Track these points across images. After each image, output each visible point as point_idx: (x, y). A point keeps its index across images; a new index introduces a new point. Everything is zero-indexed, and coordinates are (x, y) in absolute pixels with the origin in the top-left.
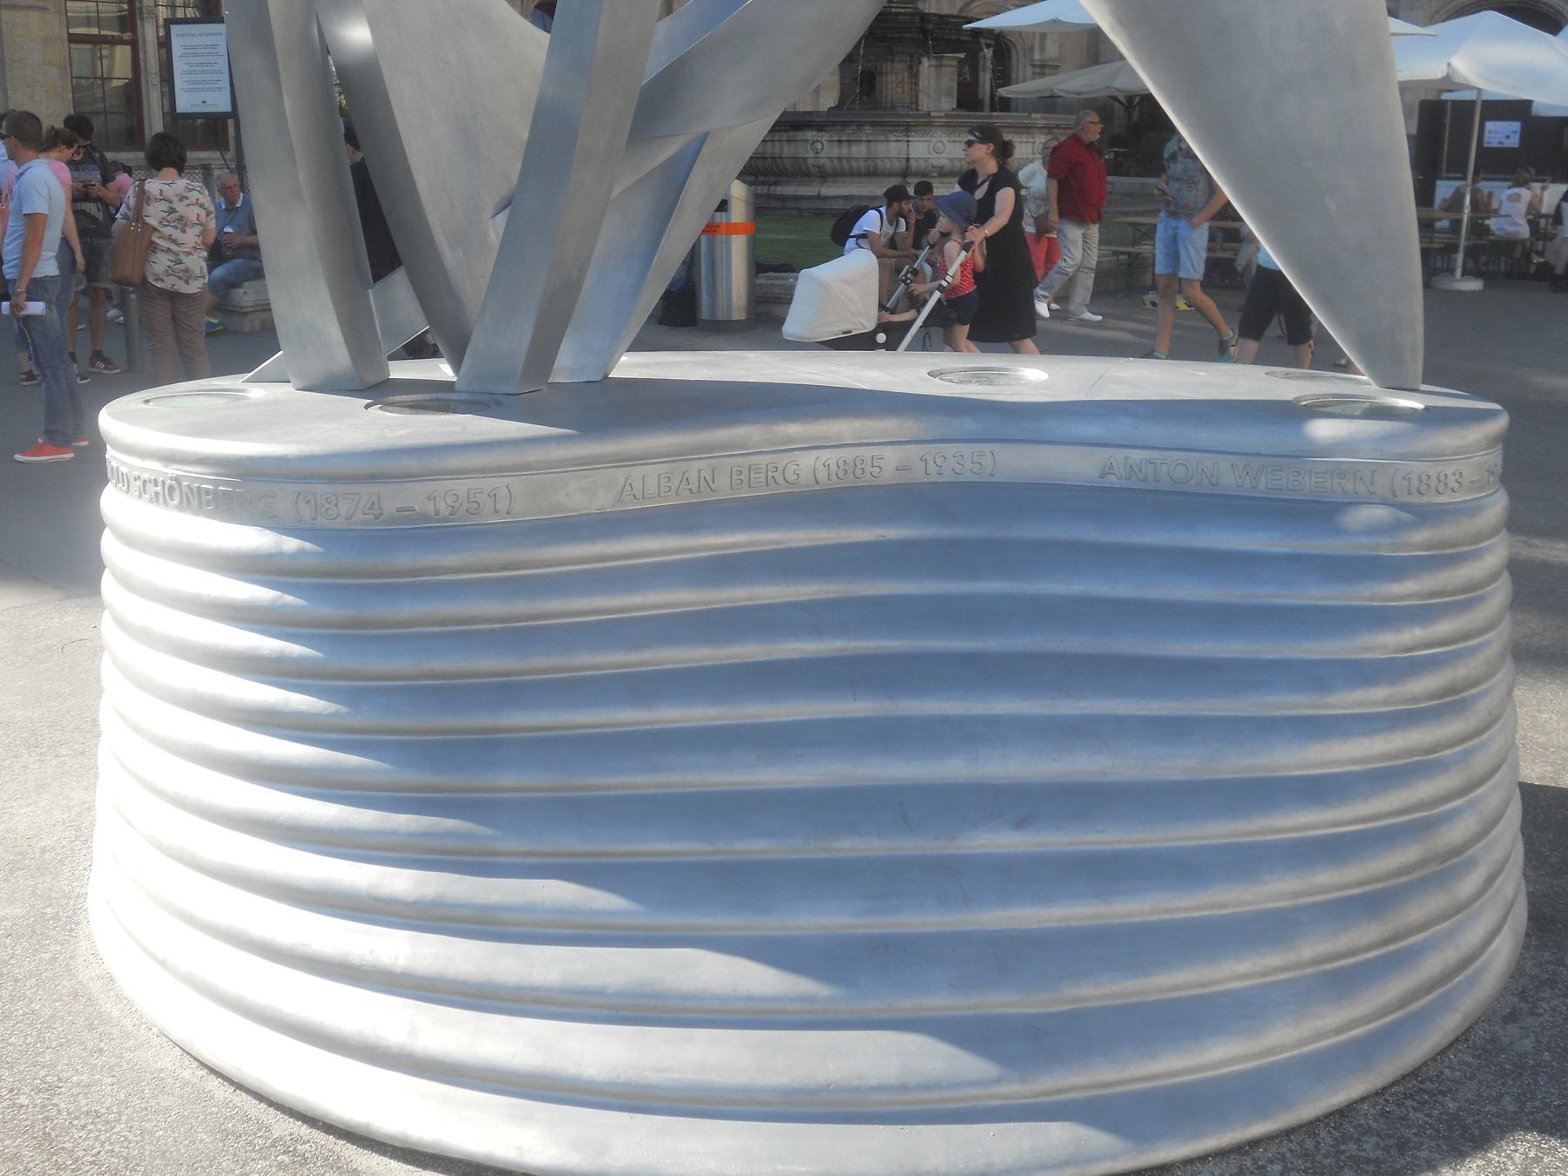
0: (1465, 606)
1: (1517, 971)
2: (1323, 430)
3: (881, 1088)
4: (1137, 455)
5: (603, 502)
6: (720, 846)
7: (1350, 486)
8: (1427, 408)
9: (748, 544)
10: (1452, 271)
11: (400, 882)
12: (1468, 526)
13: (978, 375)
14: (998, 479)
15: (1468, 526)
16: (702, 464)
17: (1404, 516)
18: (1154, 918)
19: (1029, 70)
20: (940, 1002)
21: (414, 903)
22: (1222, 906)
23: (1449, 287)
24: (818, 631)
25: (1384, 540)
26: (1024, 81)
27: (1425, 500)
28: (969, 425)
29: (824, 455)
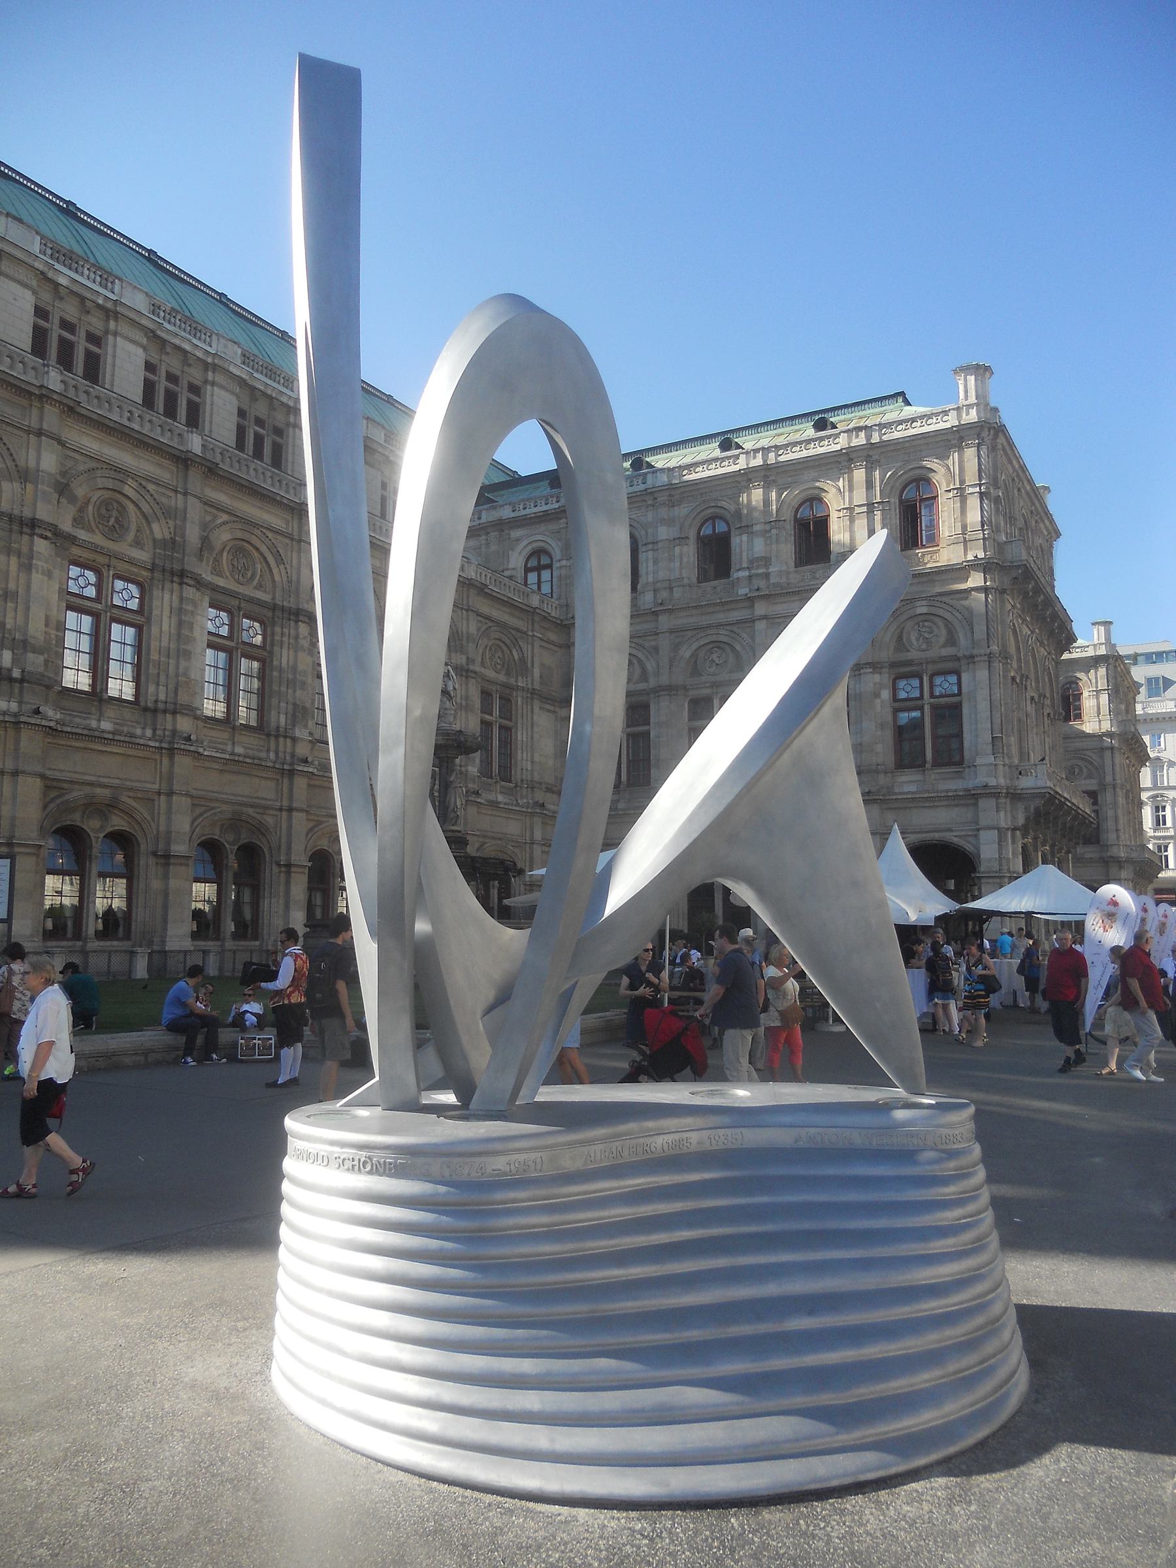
0: (974, 1198)
1: (1031, 1384)
2: (900, 1114)
3: (788, 1441)
4: (812, 1131)
5: (579, 1165)
6: (677, 1335)
7: (915, 1142)
8: (937, 1103)
9: (644, 1184)
10: (827, 1020)
11: (526, 1366)
12: (963, 1161)
13: (712, 1093)
14: (744, 1146)
15: (963, 1161)
16: (618, 1143)
17: (944, 1155)
18: (881, 1356)
19: (522, 887)
20: (800, 1401)
21: (536, 1375)
22: (910, 1348)
23: (826, 1030)
24: (690, 1226)
25: (936, 1167)
26: (519, 895)
27: (949, 1147)
28: (726, 1120)
29: (666, 1137)
